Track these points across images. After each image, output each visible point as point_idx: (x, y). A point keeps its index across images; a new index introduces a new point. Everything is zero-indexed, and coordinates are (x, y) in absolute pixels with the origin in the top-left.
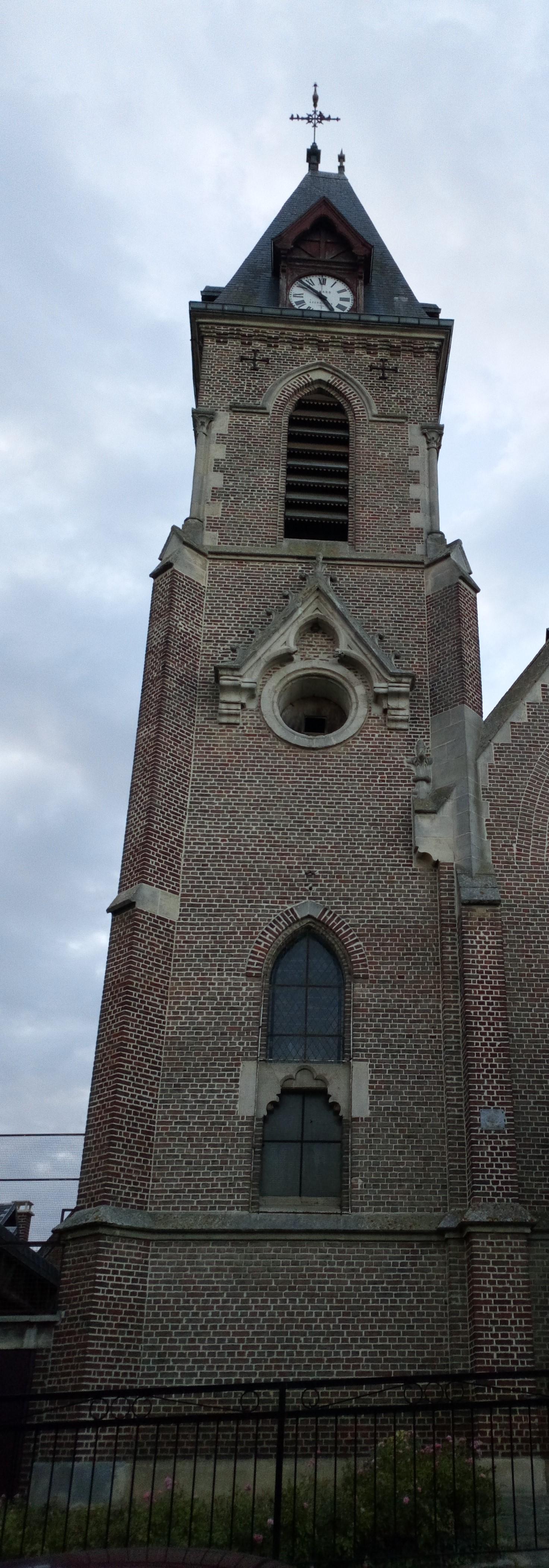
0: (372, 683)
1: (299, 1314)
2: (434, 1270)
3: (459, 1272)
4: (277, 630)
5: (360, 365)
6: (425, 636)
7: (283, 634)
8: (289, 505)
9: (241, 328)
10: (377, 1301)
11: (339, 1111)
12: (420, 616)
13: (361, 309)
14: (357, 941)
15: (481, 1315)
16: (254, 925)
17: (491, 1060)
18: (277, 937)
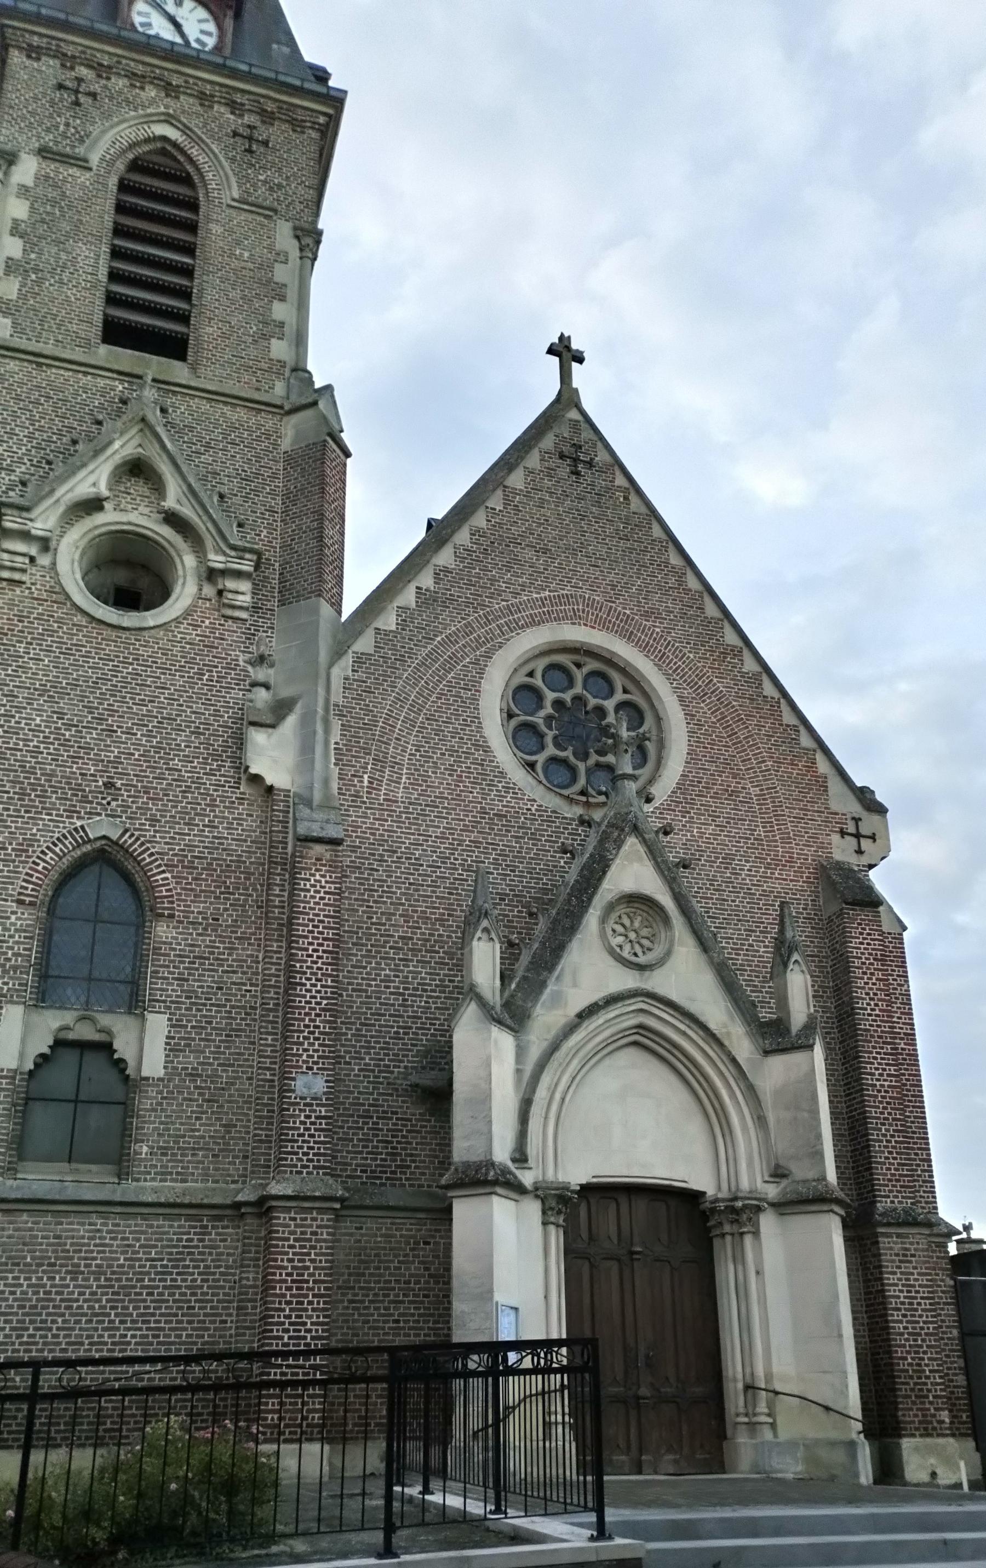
0: (205, 556)
1: (57, 1293)
2: (225, 1247)
3: (253, 1249)
4: (84, 465)
5: (221, 127)
6: (277, 503)
7: (92, 472)
8: (112, 299)
9: (62, 44)
10: (154, 1280)
11: (125, 1069)
12: (274, 476)
13: (227, 52)
14: (163, 872)
15: (276, 1295)
16: (32, 841)
17: (314, 1021)
18: (61, 858)
